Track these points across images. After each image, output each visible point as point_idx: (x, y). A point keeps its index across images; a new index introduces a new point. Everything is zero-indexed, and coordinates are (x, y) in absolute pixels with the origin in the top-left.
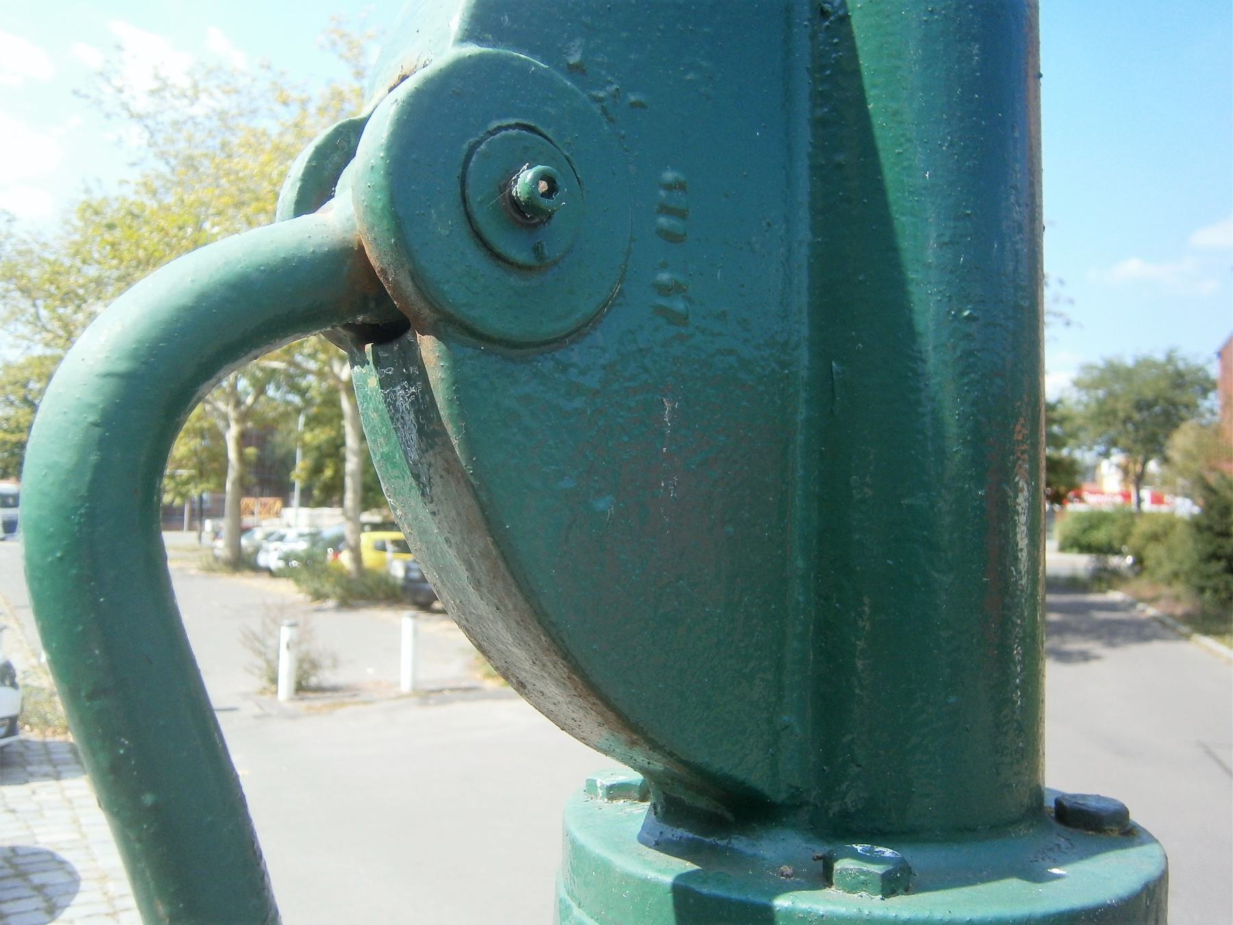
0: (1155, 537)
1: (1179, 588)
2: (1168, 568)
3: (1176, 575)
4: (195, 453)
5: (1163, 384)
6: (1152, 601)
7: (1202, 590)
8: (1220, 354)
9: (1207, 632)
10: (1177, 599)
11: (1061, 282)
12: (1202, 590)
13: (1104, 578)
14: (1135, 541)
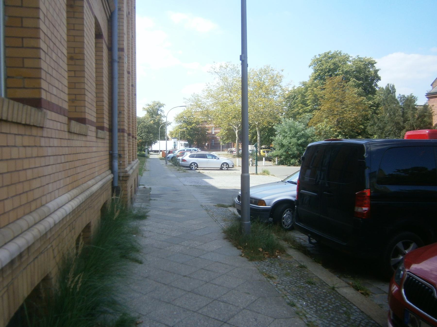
4: (226, 133)
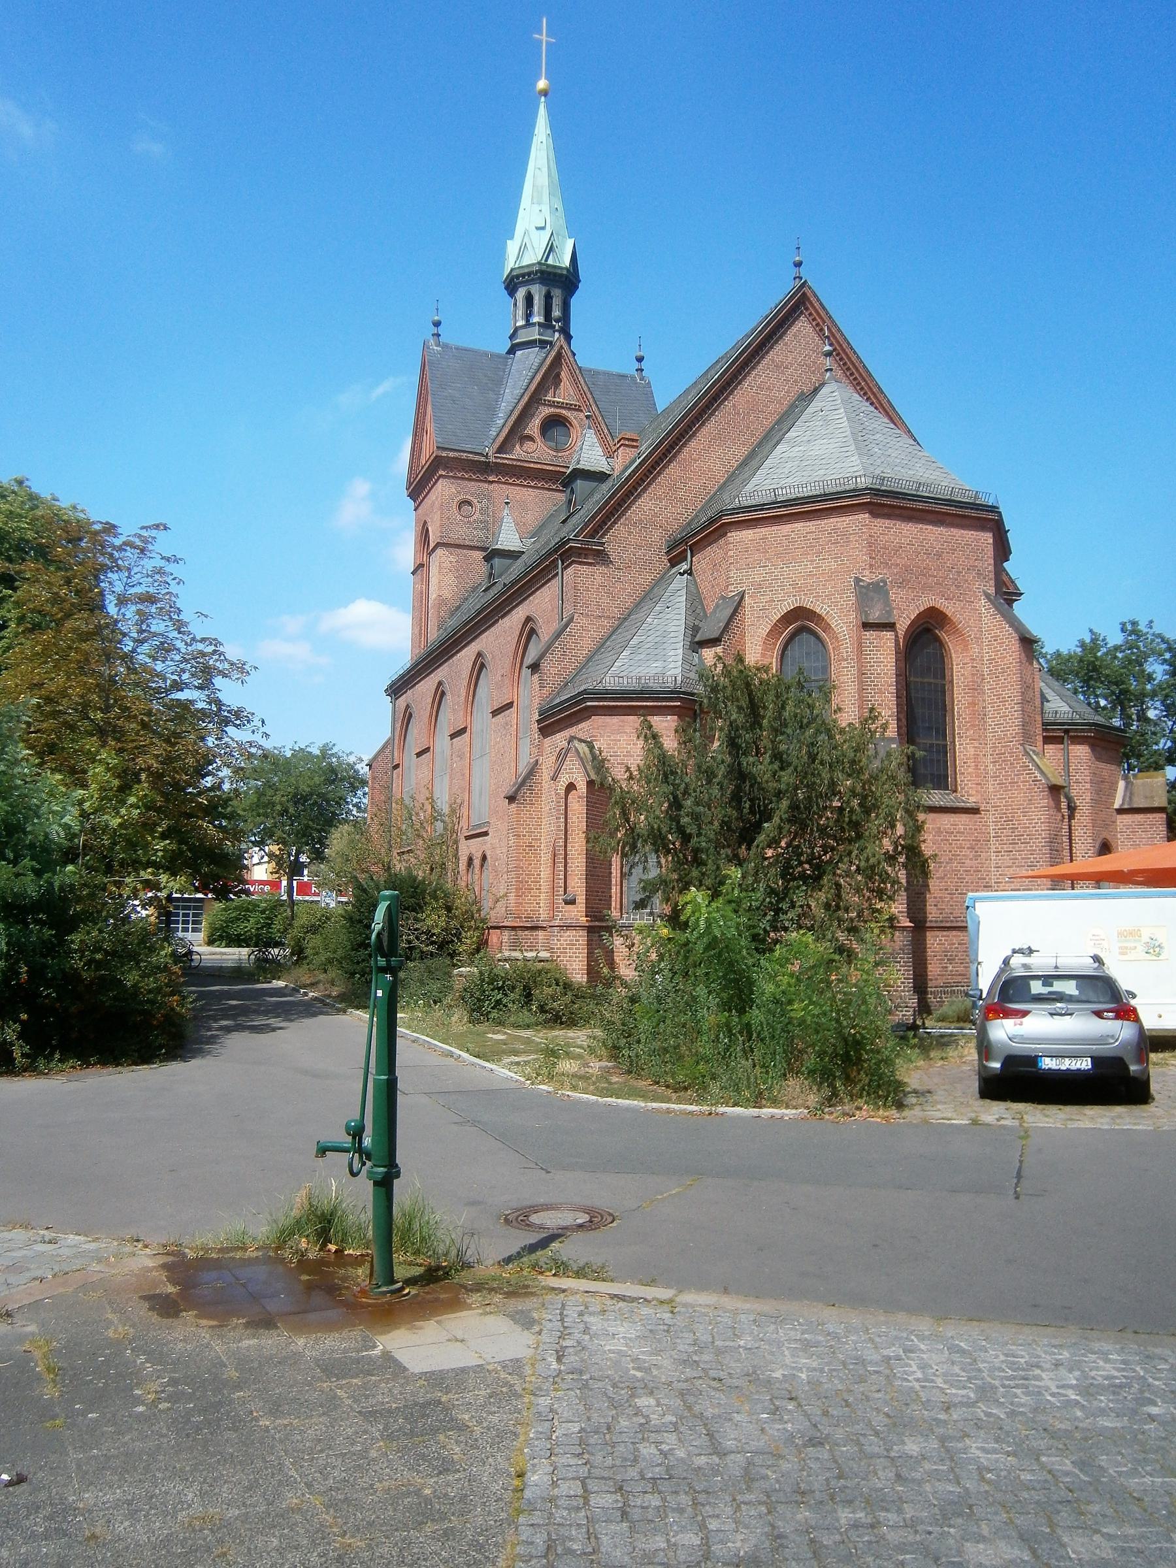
0: (313, 929)
1: (333, 973)
3: (330, 961)
7: (353, 974)
10: (332, 983)
13: (266, 968)
14: (294, 932)
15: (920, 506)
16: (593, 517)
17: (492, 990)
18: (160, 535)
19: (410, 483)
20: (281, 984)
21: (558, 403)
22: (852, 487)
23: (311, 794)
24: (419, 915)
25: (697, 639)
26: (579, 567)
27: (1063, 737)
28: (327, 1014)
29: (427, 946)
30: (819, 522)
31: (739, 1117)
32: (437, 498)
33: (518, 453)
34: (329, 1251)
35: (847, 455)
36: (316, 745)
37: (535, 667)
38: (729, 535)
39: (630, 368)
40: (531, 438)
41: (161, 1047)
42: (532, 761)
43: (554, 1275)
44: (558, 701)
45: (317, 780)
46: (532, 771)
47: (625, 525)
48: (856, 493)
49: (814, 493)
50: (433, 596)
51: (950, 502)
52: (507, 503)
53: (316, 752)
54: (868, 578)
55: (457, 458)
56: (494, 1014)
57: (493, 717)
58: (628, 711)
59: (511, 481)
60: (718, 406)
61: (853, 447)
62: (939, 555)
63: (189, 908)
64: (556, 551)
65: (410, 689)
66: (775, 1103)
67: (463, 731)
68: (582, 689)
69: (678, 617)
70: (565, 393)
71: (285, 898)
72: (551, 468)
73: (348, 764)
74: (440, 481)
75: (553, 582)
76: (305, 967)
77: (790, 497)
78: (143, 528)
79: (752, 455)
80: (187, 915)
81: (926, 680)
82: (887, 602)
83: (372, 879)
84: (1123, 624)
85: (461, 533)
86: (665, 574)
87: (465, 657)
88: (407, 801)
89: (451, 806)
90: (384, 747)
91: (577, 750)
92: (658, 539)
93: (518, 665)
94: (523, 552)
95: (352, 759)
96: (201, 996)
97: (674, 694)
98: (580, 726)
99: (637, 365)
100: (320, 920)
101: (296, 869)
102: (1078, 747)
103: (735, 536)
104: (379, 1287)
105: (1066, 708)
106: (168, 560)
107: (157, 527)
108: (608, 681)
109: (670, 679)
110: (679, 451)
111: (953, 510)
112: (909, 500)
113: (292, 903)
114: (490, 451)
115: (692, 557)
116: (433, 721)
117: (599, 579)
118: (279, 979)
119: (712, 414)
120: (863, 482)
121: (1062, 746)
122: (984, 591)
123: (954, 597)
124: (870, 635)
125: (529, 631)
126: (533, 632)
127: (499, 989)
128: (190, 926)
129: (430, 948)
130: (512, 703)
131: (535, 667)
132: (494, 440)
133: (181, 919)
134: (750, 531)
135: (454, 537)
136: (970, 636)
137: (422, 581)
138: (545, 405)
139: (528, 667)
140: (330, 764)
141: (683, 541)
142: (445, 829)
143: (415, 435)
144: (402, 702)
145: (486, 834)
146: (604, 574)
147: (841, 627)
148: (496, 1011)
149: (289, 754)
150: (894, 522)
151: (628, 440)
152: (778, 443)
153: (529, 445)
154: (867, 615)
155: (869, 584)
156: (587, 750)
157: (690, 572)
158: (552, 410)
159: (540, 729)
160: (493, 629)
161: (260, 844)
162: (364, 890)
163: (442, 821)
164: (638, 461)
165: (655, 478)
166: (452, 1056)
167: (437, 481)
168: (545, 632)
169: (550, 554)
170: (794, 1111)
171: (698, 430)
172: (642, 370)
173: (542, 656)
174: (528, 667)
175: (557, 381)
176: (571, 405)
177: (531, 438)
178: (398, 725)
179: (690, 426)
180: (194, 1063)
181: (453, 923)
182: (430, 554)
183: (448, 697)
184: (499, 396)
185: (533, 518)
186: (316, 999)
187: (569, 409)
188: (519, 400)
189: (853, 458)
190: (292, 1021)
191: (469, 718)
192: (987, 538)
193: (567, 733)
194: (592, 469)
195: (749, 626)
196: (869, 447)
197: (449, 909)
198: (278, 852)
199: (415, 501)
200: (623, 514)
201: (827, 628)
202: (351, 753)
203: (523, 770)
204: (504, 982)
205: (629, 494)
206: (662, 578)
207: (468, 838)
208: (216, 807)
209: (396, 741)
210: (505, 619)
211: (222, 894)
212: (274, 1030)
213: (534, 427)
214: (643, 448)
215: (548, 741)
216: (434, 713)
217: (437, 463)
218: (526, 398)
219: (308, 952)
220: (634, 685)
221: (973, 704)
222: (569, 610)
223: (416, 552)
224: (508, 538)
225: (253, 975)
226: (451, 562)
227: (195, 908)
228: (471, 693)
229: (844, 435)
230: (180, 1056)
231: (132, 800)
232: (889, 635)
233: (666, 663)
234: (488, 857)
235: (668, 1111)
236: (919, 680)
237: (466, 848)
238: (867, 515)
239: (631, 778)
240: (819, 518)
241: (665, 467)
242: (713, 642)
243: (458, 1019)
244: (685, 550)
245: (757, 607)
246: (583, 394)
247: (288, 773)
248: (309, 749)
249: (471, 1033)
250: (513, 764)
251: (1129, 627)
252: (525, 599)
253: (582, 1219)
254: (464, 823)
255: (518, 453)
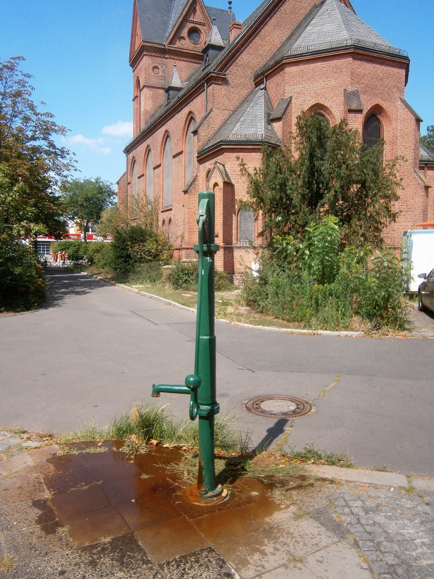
0: (97, 251)
2: (103, 262)
3: (105, 264)
5: (95, 192)
6: (99, 274)
8: (118, 183)
9: (121, 283)
11: (74, 154)
12: (116, 269)
13: (78, 267)
15: (375, 55)
16: (221, 62)
17: (183, 275)
18: (21, 62)
19: (130, 60)
20: (85, 273)
21: (195, 21)
22: (345, 45)
23: (92, 198)
24: (145, 244)
25: (270, 118)
26: (215, 86)
27: (424, 167)
28: (107, 286)
29: (149, 256)
30: (328, 62)
31: (328, 336)
32: (143, 66)
33: (178, 44)
34: (152, 444)
35: (341, 30)
36: (94, 178)
37: (195, 132)
38: (285, 69)
39: (225, 7)
40: (183, 38)
41: (35, 302)
42: (194, 175)
43: (313, 463)
44: (207, 147)
45: (95, 192)
46: (195, 180)
47: (236, 66)
48: (346, 48)
49: (326, 48)
50: (142, 109)
51: (388, 54)
52: (175, 66)
53: (93, 181)
54: (350, 89)
55: (151, 46)
56: (184, 285)
57: (174, 158)
58: (240, 150)
59: (175, 58)
60: (278, 9)
61: (344, 27)
62: (382, 79)
63: (44, 245)
64: (204, 78)
65: (134, 149)
66: (346, 328)
67: (159, 166)
68: (219, 140)
69: (261, 108)
70: (198, 17)
71: (83, 241)
72: (192, 52)
73: (107, 186)
74: (144, 57)
75: (202, 94)
76: (95, 267)
77: (315, 50)
78: (12, 58)
79: (292, 35)
80: (44, 248)
81: (372, 138)
82: (359, 101)
83: (123, 229)
84: (428, 127)
85: (154, 81)
86: (253, 90)
87: (160, 133)
88: (136, 197)
89: (154, 198)
90: (123, 177)
91: (218, 168)
92: (250, 73)
93: (185, 134)
94: (183, 88)
95: (108, 184)
96: (52, 279)
97: (262, 143)
98: (218, 158)
99: (229, 6)
100: (100, 247)
101: (86, 229)
102: (430, 171)
103: (288, 70)
104: (206, 493)
105: (426, 154)
106: (25, 75)
107: (19, 58)
108: (231, 137)
109: (260, 136)
110: (259, 32)
111: (389, 58)
112: (371, 52)
113: (87, 243)
114: (166, 43)
115: (266, 81)
116: (145, 162)
117: (224, 92)
118: (84, 271)
119: (275, 14)
120: (350, 43)
121: (423, 171)
122: (400, 98)
123: (387, 99)
124: (351, 115)
125: (191, 118)
126: (192, 118)
127: (186, 274)
128: (46, 252)
129: (150, 258)
130: (182, 151)
131: (195, 132)
132: (167, 38)
133: (42, 249)
134: (295, 67)
135: (151, 83)
136: (393, 118)
137: (137, 103)
138: (189, 22)
139: (192, 133)
140: (100, 186)
141: (262, 74)
142: (152, 208)
143: (132, 36)
144: (131, 156)
145: (171, 210)
146: (226, 90)
147: (337, 113)
148: (185, 284)
149: (82, 182)
150: (363, 62)
151: (237, 25)
152: (307, 26)
153: (182, 41)
154: (350, 106)
155: (351, 92)
156: (222, 168)
157: (265, 89)
158: (193, 25)
159: (198, 161)
160: (173, 119)
161: (73, 219)
162: (120, 234)
163: (151, 205)
164: (241, 36)
165: (249, 44)
166: (171, 305)
167: (143, 57)
168: (198, 118)
169: (201, 80)
170: (357, 333)
171: (268, 21)
172: (231, 8)
173: (199, 127)
174: (192, 133)
175: (195, 11)
176: (201, 23)
177: (183, 38)
178: (130, 166)
179: (265, 19)
180: (51, 309)
181: (160, 247)
182: (140, 91)
183: (152, 151)
184: (169, 18)
185: (185, 74)
186: (101, 279)
187: (200, 25)
188: (178, 20)
189: (344, 32)
190: (93, 289)
191: (162, 160)
192: (403, 72)
193: (213, 161)
194: (216, 44)
195: (294, 112)
196: (350, 28)
197: (157, 241)
198: (79, 222)
199: (133, 68)
200: (234, 61)
201: (330, 113)
202: (108, 181)
203: (189, 179)
204: (188, 272)
205: (237, 51)
206: (252, 92)
207: (162, 212)
208: (54, 200)
209: (129, 173)
210: (178, 114)
211: (58, 237)
212: (86, 293)
213: (185, 33)
214: (243, 30)
215: (202, 166)
216: (146, 159)
217: (143, 49)
218: (181, 19)
219: (96, 261)
220: (243, 139)
221: (392, 150)
222: (210, 106)
223: (134, 91)
224: (176, 82)
225: (73, 270)
226: (150, 94)
227: (47, 245)
228: (163, 148)
229: (339, 21)
230: (44, 307)
231: (15, 189)
232: (359, 115)
233: (257, 129)
234: (172, 219)
235: (292, 333)
236: (369, 138)
237: (162, 216)
238: (351, 59)
239: (256, 173)
240: (328, 60)
241: (253, 39)
242: (278, 119)
243: (168, 288)
244: (263, 78)
245: (298, 103)
246: (206, 17)
247: (82, 189)
248: (90, 180)
249: (175, 294)
250: (183, 179)
251: (431, 128)
252: (188, 103)
253: (293, 407)
254: (161, 206)
255: (178, 44)
